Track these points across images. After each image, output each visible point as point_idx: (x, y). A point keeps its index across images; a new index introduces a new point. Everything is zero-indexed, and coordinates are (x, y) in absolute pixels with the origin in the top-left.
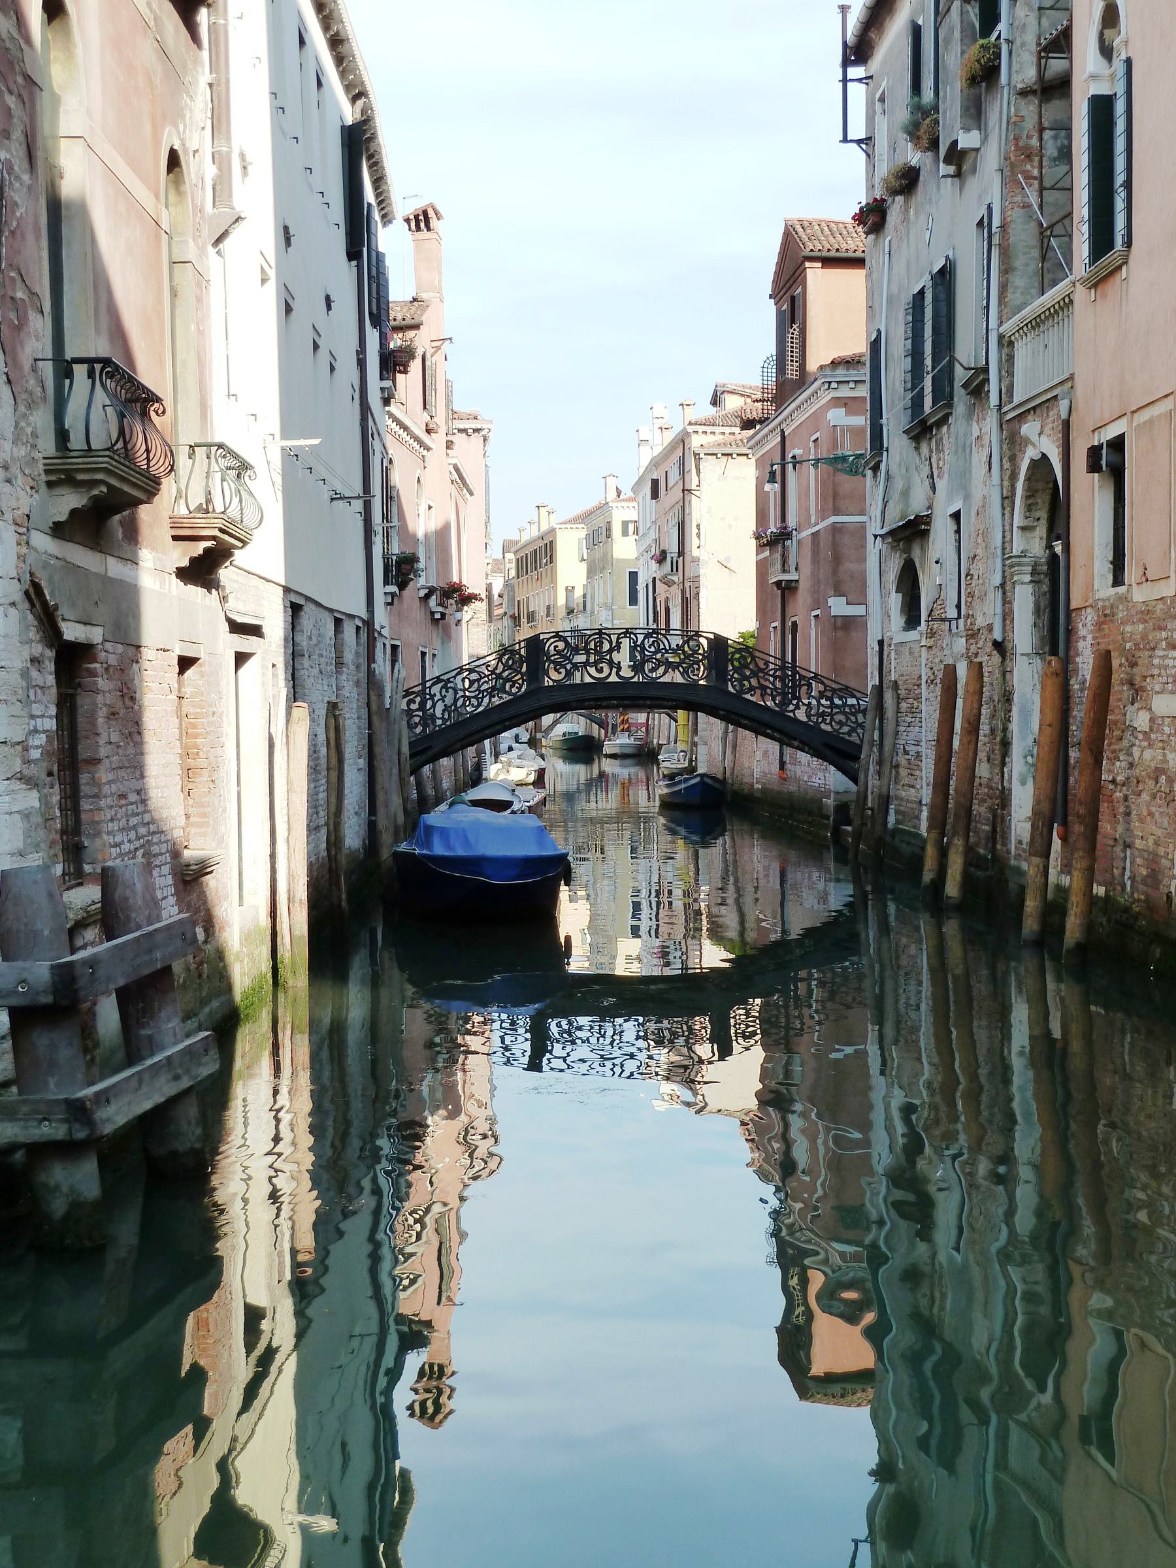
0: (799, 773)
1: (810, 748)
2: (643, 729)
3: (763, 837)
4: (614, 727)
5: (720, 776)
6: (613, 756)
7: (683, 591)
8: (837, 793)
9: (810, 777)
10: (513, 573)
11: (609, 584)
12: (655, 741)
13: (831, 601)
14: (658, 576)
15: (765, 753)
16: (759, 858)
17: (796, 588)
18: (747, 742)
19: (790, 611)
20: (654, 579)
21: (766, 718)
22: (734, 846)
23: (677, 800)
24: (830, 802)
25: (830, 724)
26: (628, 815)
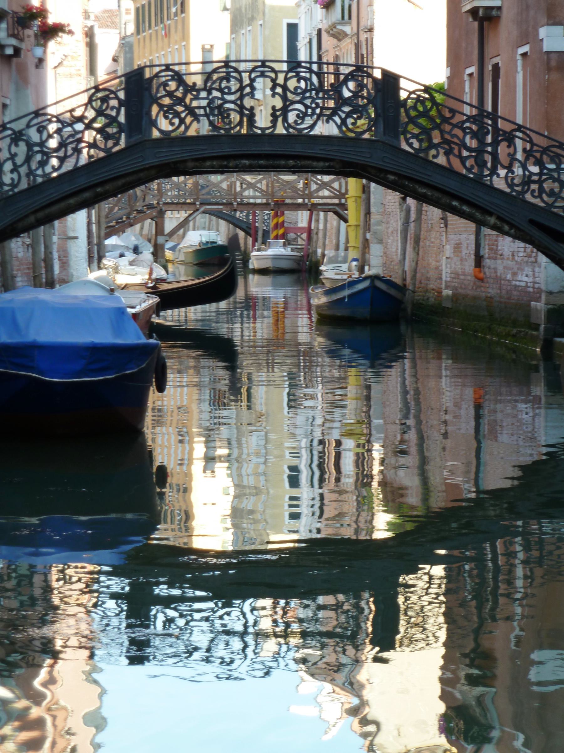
0: (500, 269)
1: (512, 226)
2: (304, 236)
3: (455, 358)
4: (266, 234)
5: (398, 281)
6: (263, 272)
7: (358, 46)
8: (550, 293)
9: (515, 274)
10: (131, 28)
11: (260, 39)
12: (319, 251)
13: (543, 32)
14: (324, 26)
15: (457, 247)
16: (448, 388)
17: (498, 18)
18: (433, 234)
19: (489, 50)
20: (319, 31)
21: (452, 185)
22: (415, 375)
23: (339, 313)
24: (540, 306)
25: (540, 196)
26: (280, 343)
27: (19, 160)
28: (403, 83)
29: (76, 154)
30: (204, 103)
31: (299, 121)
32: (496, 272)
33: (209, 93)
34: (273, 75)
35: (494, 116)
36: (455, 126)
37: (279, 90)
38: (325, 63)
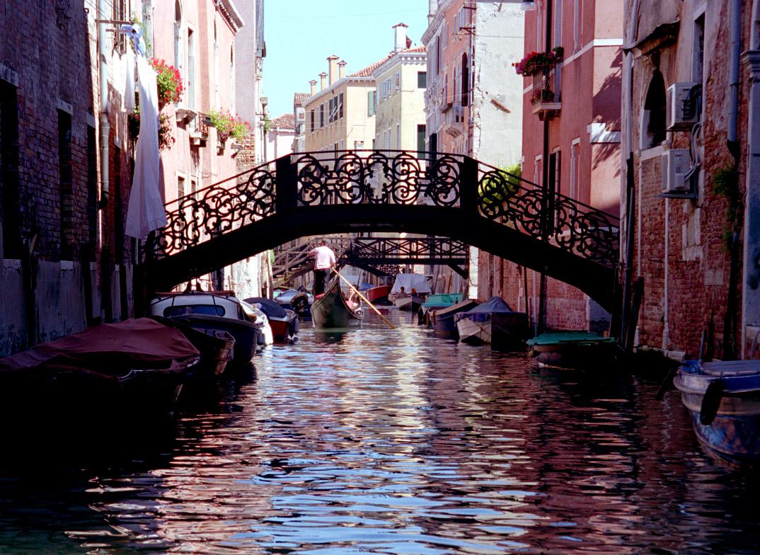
27: (200, 222)
28: (481, 167)
29: (241, 219)
30: (334, 181)
31: (405, 195)
32: (555, 307)
33: (338, 174)
34: (384, 161)
35: (553, 193)
36: (519, 199)
37: (390, 172)
38: (427, 152)
